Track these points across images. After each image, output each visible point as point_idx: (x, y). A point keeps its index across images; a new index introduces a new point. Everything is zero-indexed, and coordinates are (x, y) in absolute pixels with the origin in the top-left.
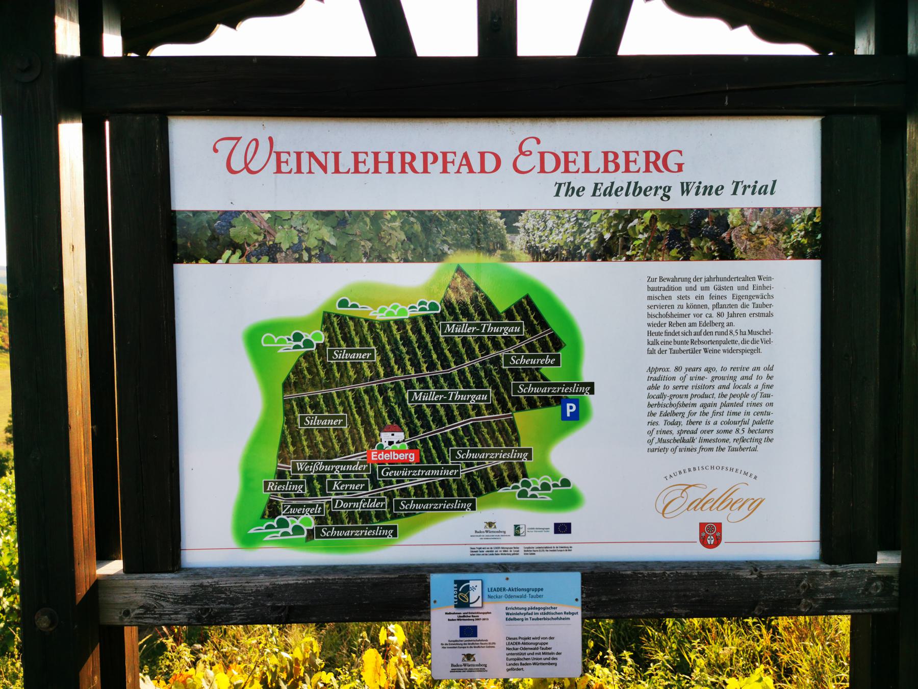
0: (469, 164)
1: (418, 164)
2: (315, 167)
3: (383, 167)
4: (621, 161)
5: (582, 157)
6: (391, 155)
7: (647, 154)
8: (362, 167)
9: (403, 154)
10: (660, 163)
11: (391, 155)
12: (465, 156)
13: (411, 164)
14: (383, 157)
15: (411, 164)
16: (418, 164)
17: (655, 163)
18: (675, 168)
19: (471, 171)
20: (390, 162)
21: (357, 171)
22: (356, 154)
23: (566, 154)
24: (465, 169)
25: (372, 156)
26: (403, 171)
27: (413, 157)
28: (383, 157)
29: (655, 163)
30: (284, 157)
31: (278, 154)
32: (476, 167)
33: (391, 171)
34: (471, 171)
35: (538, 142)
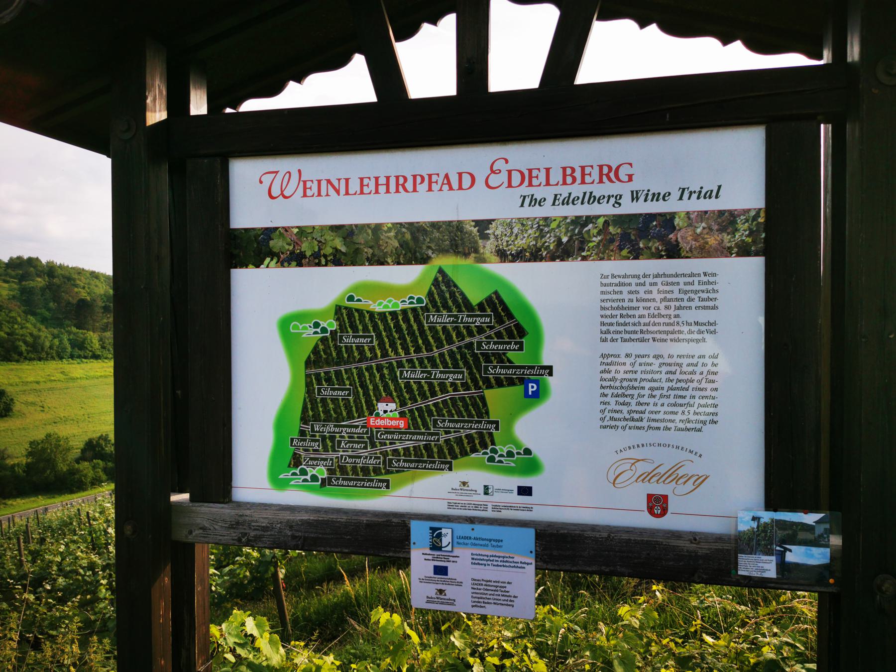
0: (449, 183)
1: (409, 185)
2: (331, 191)
3: (382, 189)
4: (578, 174)
5: (543, 172)
6: (388, 178)
7: (601, 167)
8: (366, 190)
9: (397, 178)
10: (612, 175)
11: (388, 178)
12: (447, 176)
13: (403, 186)
14: (382, 181)
15: (403, 186)
16: (409, 185)
17: (608, 176)
18: (626, 179)
19: (451, 189)
20: (388, 185)
21: (362, 193)
22: (362, 179)
23: (530, 171)
24: (446, 187)
25: (597, 169)
26: (397, 191)
27: (573, 170)
28: (382, 181)
29: (608, 176)
30: (309, 184)
31: (305, 182)
32: (455, 185)
33: (388, 191)
34: (451, 189)
35: (507, 162)
